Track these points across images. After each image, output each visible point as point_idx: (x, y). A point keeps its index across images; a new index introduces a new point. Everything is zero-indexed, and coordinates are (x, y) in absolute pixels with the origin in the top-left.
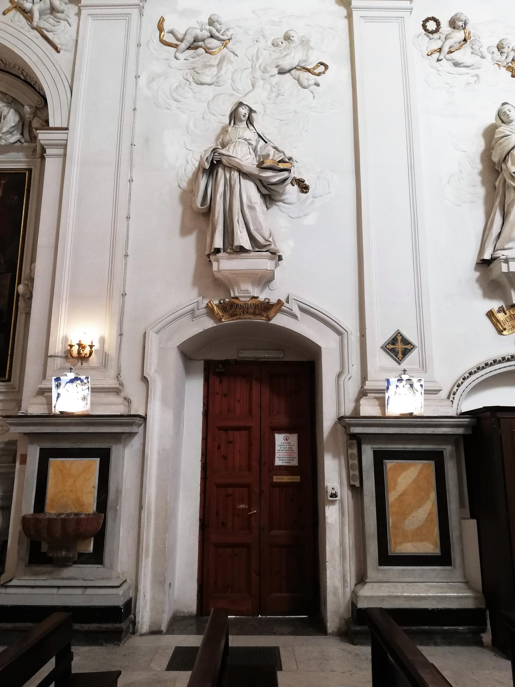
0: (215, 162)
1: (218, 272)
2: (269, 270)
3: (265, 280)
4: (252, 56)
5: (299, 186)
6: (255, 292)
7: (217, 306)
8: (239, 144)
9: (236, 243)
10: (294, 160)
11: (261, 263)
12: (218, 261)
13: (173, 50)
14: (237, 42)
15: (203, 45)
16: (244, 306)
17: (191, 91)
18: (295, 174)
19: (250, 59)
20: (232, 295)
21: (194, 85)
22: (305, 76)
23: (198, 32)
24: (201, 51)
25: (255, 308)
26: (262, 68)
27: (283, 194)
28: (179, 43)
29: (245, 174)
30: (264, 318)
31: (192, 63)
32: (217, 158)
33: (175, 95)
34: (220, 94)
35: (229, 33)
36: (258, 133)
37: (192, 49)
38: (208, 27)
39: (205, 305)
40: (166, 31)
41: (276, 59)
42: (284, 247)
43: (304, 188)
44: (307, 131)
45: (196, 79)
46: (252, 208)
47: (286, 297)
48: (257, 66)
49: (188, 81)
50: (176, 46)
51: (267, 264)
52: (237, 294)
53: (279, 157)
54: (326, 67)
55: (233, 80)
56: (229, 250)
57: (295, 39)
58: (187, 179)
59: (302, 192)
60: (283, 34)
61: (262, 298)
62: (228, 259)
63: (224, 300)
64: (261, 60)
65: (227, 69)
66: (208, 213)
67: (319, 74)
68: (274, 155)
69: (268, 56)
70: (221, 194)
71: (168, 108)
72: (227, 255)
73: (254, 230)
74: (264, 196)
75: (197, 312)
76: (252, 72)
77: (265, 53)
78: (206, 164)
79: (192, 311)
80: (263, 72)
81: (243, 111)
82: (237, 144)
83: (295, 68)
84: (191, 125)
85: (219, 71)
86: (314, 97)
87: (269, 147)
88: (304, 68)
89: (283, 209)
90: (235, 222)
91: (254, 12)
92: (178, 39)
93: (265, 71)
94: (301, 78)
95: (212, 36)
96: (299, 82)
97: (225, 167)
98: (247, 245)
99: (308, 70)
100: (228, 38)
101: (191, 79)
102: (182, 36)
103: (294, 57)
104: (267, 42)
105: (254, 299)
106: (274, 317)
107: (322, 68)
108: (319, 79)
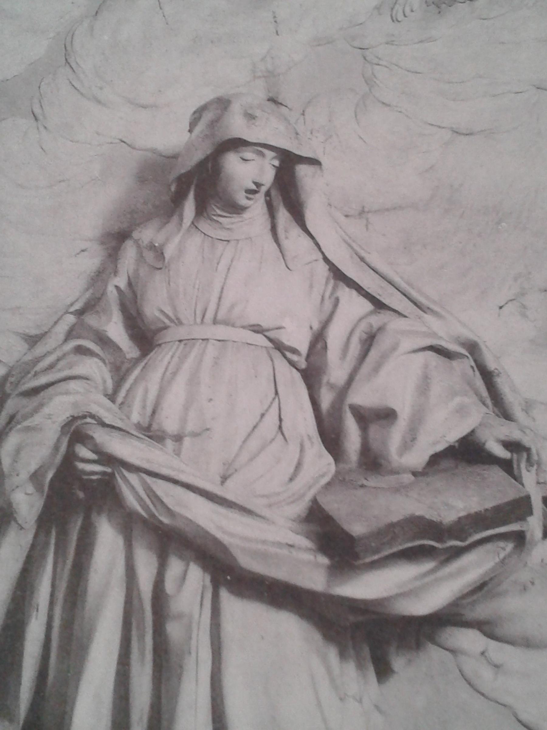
36: (326, 260)
81: (247, 172)
97: (130, 524)
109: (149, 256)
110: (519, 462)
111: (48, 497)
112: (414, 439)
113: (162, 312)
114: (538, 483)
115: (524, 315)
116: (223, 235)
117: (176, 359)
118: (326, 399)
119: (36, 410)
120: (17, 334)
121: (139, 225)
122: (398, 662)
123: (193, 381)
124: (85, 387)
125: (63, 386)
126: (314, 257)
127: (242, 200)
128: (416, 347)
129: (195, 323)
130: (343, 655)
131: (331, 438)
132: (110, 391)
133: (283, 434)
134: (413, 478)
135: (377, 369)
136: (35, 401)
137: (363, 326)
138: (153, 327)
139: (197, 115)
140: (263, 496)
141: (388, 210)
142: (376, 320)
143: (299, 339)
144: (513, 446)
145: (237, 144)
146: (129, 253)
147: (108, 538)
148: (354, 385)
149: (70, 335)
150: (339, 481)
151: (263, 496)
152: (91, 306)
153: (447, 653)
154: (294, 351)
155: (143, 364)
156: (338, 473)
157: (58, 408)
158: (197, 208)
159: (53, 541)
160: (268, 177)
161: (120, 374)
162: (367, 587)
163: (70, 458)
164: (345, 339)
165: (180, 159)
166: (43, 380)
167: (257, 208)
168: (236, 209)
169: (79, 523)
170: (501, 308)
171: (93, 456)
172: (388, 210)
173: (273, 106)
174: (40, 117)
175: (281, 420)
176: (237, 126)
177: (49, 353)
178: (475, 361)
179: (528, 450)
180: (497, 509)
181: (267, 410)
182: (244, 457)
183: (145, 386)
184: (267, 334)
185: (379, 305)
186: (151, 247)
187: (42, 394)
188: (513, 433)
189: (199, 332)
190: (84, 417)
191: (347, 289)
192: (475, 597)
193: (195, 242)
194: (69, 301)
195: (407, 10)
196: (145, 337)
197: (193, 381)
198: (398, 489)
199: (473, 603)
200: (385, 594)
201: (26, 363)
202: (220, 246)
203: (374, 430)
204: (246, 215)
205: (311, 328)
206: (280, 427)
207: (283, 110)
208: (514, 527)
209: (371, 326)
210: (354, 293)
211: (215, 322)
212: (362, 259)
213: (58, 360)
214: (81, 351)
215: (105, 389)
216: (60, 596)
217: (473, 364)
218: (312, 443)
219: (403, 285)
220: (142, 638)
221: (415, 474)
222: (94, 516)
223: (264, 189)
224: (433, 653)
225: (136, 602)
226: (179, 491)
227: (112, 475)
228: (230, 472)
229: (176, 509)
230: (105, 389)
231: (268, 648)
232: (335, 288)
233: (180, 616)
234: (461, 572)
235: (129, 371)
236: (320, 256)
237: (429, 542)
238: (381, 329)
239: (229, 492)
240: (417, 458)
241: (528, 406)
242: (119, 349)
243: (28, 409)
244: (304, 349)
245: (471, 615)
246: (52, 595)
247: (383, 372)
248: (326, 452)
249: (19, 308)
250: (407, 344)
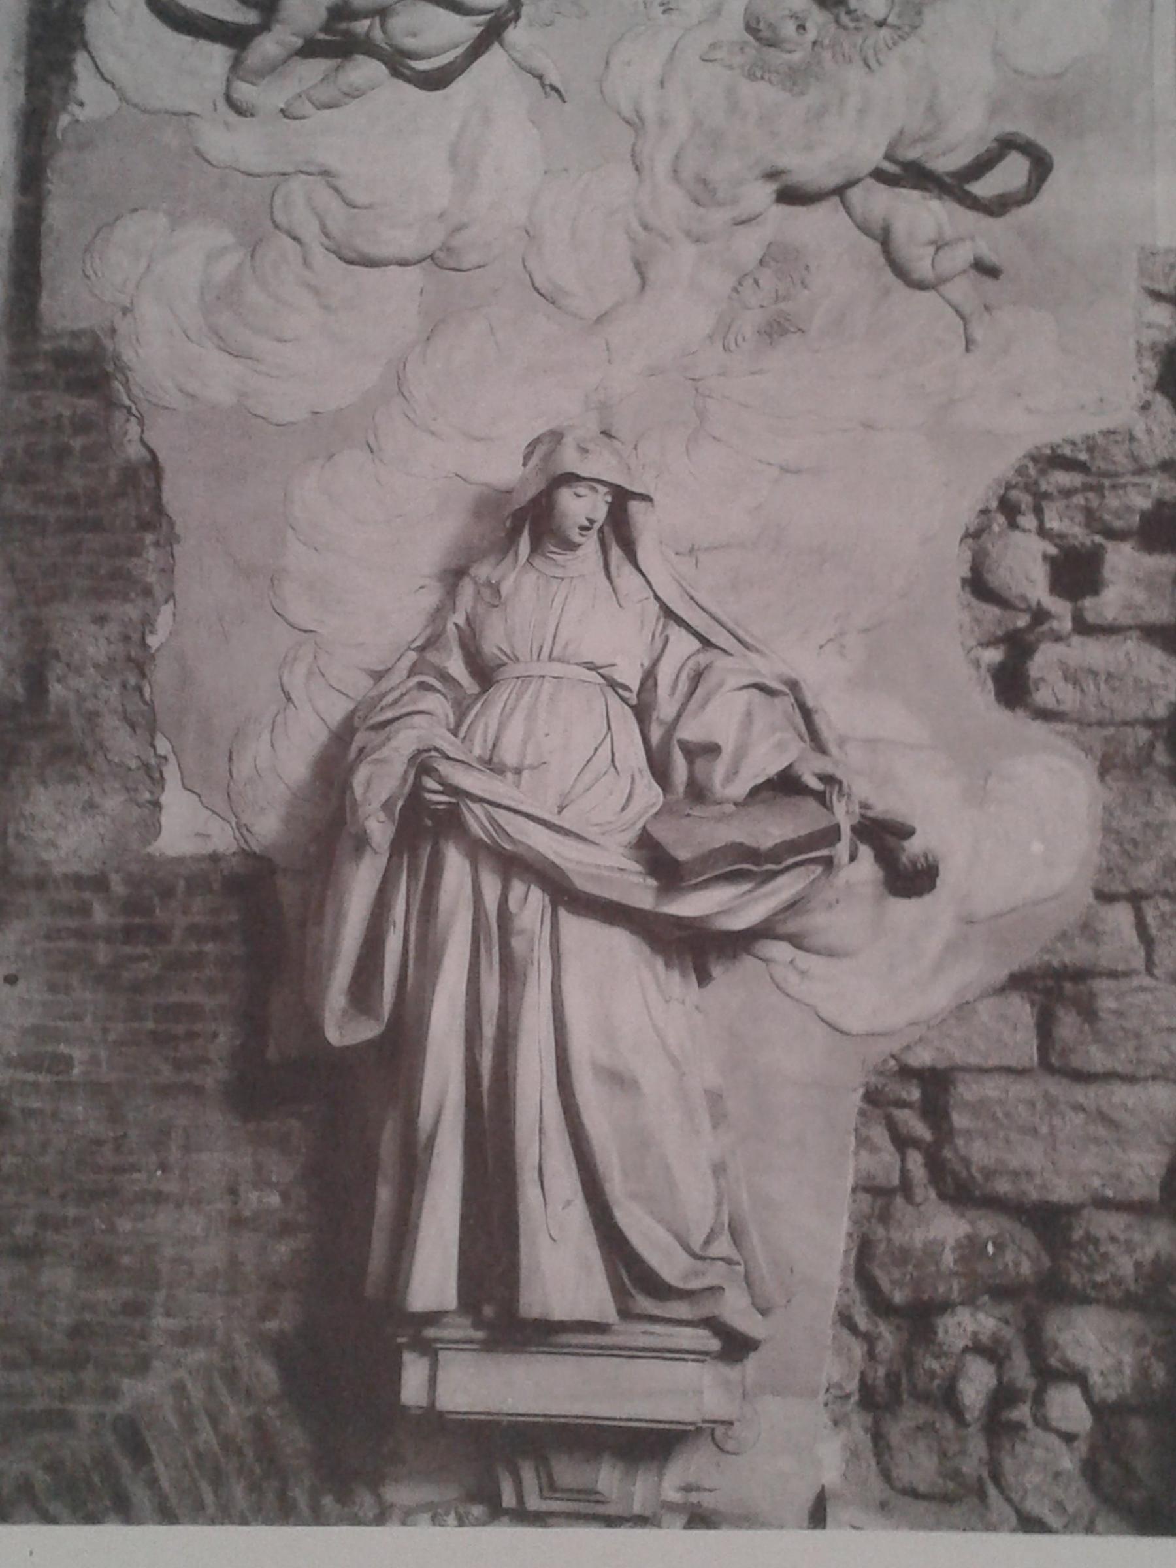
22: (919, 216)
36: (657, 598)
67: (998, 207)
80: (698, 202)
81: (581, 507)
93: (703, 192)
97: (475, 850)
109: (487, 593)
110: (831, 794)
111: (399, 824)
112: (736, 773)
113: (501, 650)
114: (847, 812)
115: (842, 655)
116: (559, 572)
117: (514, 696)
118: (656, 735)
119: (383, 744)
120: (364, 670)
121: (475, 562)
122: (716, 971)
123: (531, 717)
124: (427, 724)
125: (408, 720)
126: (645, 596)
127: (577, 539)
128: (741, 684)
129: (532, 660)
130: (668, 965)
131: (660, 771)
132: (452, 727)
133: (616, 768)
134: (733, 808)
135: (703, 706)
136: (383, 734)
137: (691, 664)
138: (491, 664)
139: (530, 448)
140: (597, 825)
141: (716, 548)
142: (703, 658)
144: (828, 779)
145: (570, 479)
146: (467, 590)
147: (455, 864)
148: (683, 720)
149: (412, 672)
150: (666, 810)
151: (597, 825)
152: (432, 642)
153: (759, 962)
154: (626, 688)
155: (482, 700)
156: (664, 805)
157: (404, 742)
158: (532, 543)
159: (405, 865)
160: (601, 514)
161: (461, 709)
162: (691, 905)
163: (416, 795)
164: (674, 677)
165: (514, 494)
166: (389, 715)
167: (590, 545)
168: (572, 546)
169: (429, 848)
170: (821, 647)
171: (440, 788)
172: (716, 548)
173: (606, 439)
174: (375, 449)
175: (613, 754)
176: (570, 461)
177: (392, 689)
178: (797, 700)
179: (840, 783)
180: (811, 836)
181: (600, 745)
182: (580, 787)
183: (485, 723)
184: (601, 671)
185: (706, 643)
186: (489, 584)
187: (387, 729)
188: (824, 765)
189: (535, 669)
190: (429, 750)
191: (677, 628)
192: (788, 914)
193: (530, 579)
194: (410, 638)
195: (740, 339)
196: (485, 674)
197: (531, 717)
198: (724, 818)
199: (784, 921)
200: (707, 912)
201: (372, 698)
202: (555, 582)
203: (700, 763)
204: (580, 552)
205: (642, 665)
206: (613, 760)
207: (616, 443)
208: (824, 852)
209: (699, 664)
210: (683, 632)
212: (692, 598)
213: (403, 695)
214: (423, 686)
215: (448, 724)
216: (414, 913)
217: (793, 700)
218: (642, 777)
219: (731, 625)
220: (489, 951)
221: (736, 804)
222: (442, 842)
223: (597, 526)
224: (748, 963)
225: (483, 920)
226: (520, 819)
227: (458, 804)
228: (566, 802)
229: (517, 836)
230: (448, 724)
231: (602, 958)
232: (664, 627)
233: (521, 932)
234: (773, 893)
235: (469, 708)
236: (651, 594)
237: (747, 865)
238: (708, 667)
239: (565, 821)
240: (739, 789)
241: (842, 742)
242: (460, 685)
243: (376, 743)
244: (635, 686)
245: (782, 929)
246: (407, 912)
247: (710, 708)
248: (655, 785)
249: (362, 644)
250: (732, 681)
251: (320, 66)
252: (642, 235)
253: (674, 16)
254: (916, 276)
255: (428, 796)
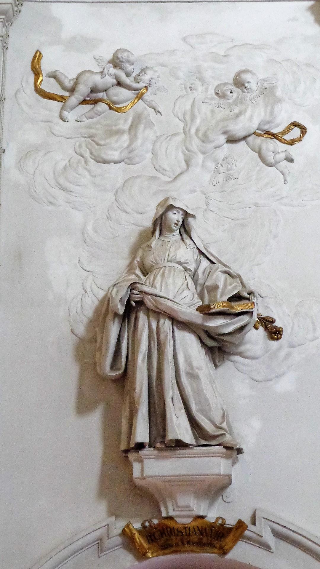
0: (133, 304)
1: (141, 479)
2: (223, 475)
3: (217, 489)
4: (184, 115)
5: (266, 328)
6: (199, 507)
7: (140, 532)
8: (170, 271)
9: (171, 436)
10: (257, 294)
11: (209, 464)
12: (141, 461)
13: (56, 105)
14: (158, 90)
15: (105, 97)
16: (184, 531)
17: (86, 173)
18: (261, 310)
19: (181, 117)
20: (164, 514)
21: (92, 162)
23: (97, 79)
24: (102, 107)
25: (202, 534)
26: (200, 134)
27: (241, 343)
28: (67, 94)
29: (179, 323)
30: (216, 550)
31: (88, 127)
32: (137, 297)
33: (62, 181)
34: (135, 178)
35: (146, 78)
36: (197, 248)
37: (88, 104)
38: (112, 71)
39: (119, 531)
40: (44, 74)
41: (223, 120)
42: (247, 432)
43: (275, 333)
44: (275, 237)
45: (95, 153)
46: (193, 376)
47: (252, 513)
48: (193, 131)
49: (82, 156)
50: (62, 99)
51: (220, 465)
52: (171, 513)
53: (234, 289)
54: (304, 130)
55: (154, 154)
56: (158, 445)
57: (253, 85)
58: (85, 320)
59: (272, 339)
60: (232, 76)
61: (212, 516)
62: (157, 458)
63: (150, 521)
64: (198, 121)
65: (146, 135)
66: (124, 380)
67: (292, 142)
68: (225, 286)
69: (207, 112)
70: (144, 355)
71: (51, 203)
72: (156, 452)
73: (198, 411)
74: (210, 351)
75: (107, 543)
76: (184, 141)
77: (205, 109)
78: (119, 306)
79: (99, 543)
80: (203, 142)
81: (175, 217)
82: (167, 272)
83: (254, 133)
84: (89, 229)
85: (132, 141)
86: (285, 180)
87: (217, 273)
88: (268, 133)
89: (242, 367)
90: (168, 401)
91: (184, 39)
92: (64, 88)
93: (205, 139)
94: (264, 151)
95: (119, 84)
96: (260, 156)
97: (148, 311)
98: (187, 437)
99: (275, 136)
100: (144, 85)
101: (87, 154)
102: (72, 83)
103: (251, 118)
104: (207, 90)
105: (199, 521)
106: (232, 547)
107: (296, 132)
108: (292, 150)
116: (168, 240)
143: (192, 267)
169: (134, 316)
203: (212, 295)
211: (168, 262)
232: (200, 257)
251: (89, 107)
252: (187, 152)
253: (194, 91)
254: (268, 161)
255: (134, 295)
